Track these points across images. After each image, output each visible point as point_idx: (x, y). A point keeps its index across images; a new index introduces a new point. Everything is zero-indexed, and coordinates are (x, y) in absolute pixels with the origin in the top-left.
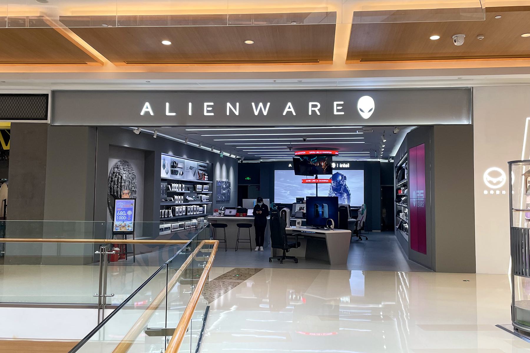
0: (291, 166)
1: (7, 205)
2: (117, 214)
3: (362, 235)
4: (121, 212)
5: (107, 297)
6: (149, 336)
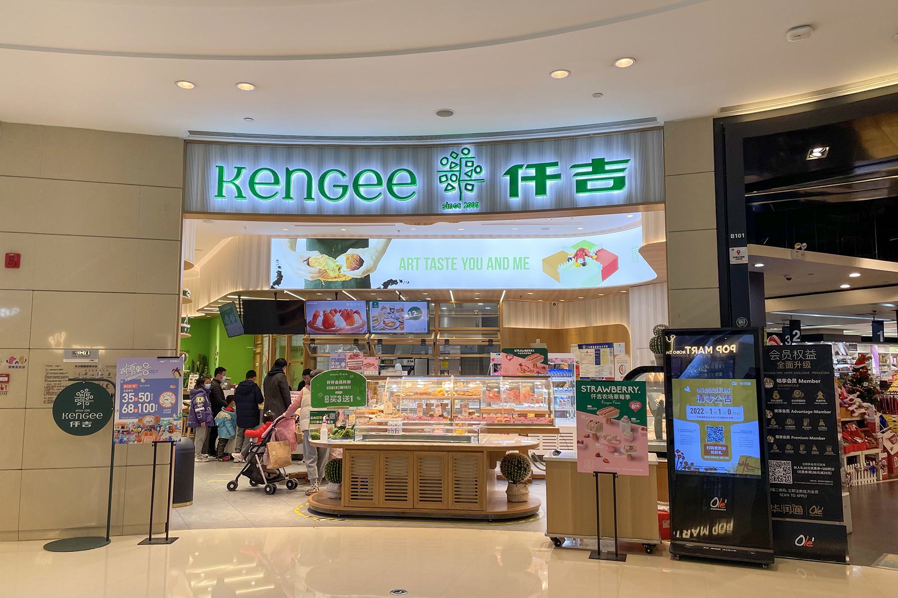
0: (685, 389)
1: (193, 370)
2: (123, 411)
3: (454, 170)
4: (131, 407)
5: (158, 443)
6: (247, 373)
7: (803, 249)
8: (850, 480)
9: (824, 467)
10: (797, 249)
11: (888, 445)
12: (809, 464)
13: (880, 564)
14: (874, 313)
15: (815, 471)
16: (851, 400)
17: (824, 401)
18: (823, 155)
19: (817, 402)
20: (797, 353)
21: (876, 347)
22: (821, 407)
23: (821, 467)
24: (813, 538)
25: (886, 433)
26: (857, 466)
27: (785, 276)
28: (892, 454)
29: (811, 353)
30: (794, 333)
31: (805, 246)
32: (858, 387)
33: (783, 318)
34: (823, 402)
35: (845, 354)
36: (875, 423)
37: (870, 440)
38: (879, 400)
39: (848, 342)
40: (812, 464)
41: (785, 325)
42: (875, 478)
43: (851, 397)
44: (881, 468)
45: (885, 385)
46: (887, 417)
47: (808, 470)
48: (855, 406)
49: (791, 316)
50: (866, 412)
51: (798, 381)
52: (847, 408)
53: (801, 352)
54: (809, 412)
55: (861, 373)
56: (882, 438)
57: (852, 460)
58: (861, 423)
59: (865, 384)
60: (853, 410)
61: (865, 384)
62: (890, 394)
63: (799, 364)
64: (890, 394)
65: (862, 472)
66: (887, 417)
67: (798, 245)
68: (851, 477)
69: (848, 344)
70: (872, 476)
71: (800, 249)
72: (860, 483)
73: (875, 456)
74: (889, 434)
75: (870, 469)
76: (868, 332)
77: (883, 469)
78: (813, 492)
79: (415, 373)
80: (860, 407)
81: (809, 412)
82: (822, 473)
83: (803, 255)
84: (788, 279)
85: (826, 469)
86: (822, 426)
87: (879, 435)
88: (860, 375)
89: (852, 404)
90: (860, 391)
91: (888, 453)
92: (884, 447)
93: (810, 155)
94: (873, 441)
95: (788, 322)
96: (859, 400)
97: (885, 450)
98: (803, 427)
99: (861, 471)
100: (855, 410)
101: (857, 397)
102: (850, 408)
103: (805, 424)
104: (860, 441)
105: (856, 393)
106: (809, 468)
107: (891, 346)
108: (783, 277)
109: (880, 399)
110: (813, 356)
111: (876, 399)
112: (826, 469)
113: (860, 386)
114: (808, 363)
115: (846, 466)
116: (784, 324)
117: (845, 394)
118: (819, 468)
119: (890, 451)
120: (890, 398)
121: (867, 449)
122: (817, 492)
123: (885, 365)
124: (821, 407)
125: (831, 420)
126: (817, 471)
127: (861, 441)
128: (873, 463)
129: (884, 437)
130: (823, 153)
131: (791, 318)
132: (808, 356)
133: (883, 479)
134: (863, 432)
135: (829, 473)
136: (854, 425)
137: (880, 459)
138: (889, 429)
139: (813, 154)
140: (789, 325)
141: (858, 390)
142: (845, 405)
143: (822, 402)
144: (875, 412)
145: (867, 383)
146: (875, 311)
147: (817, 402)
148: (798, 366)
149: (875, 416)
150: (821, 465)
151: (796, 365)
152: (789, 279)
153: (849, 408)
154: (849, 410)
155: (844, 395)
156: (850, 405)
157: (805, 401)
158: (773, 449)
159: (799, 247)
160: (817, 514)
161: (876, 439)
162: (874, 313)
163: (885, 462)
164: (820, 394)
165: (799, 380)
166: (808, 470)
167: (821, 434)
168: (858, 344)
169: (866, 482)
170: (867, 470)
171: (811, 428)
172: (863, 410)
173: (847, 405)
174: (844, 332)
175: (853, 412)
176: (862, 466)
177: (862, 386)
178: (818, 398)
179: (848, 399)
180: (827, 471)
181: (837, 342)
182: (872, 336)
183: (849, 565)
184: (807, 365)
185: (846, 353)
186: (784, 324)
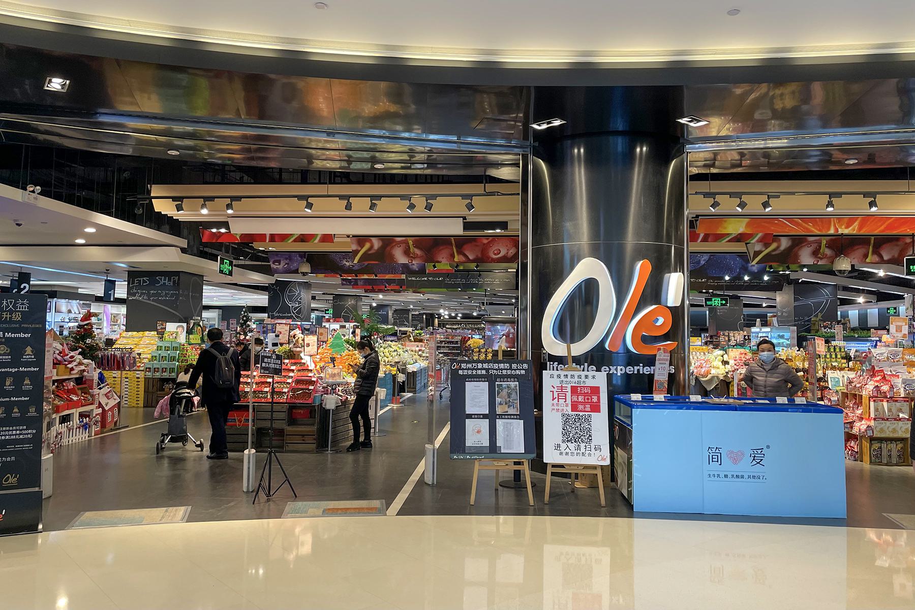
7: (36, 193)
8: (61, 440)
9: (24, 430)
10: (30, 192)
11: (103, 401)
12: (8, 428)
13: (74, 525)
14: (107, 272)
15: (13, 435)
16: (72, 357)
17: (33, 357)
18: (62, 88)
19: (25, 358)
20: (7, 303)
21: (109, 306)
22: (28, 364)
23: (20, 430)
24: (4, 510)
25: (103, 389)
26: (70, 425)
27: (15, 220)
28: (107, 409)
29: (23, 304)
30: (22, 287)
31: (39, 189)
32: (81, 344)
33: (13, 269)
34: (31, 358)
35: (77, 312)
36: (93, 380)
37: (86, 397)
38: (100, 357)
39: (82, 300)
40: (11, 428)
41: (14, 278)
42: (87, 434)
43: (72, 354)
44: (94, 424)
45: (110, 342)
46: (106, 374)
47: (5, 435)
48: (75, 363)
49: (21, 267)
50: (86, 368)
51: (4, 335)
52: (66, 365)
53: (11, 302)
54: (14, 370)
55: (85, 330)
56: (98, 394)
57: (65, 419)
58: (80, 381)
59: (88, 341)
60: (72, 367)
61: (88, 341)
62: (112, 351)
63: (8, 316)
64: (112, 351)
65: (74, 430)
66: (106, 374)
67: (32, 187)
68: (62, 436)
69: (81, 302)
70: (84, 433)
71: (33, 192)
72: (70, 442)
73: (90, 412)
74: (106, 390)
75: (82, 426)
76: (100, 292)
77: (96, 425)
78: (9, 459)
79: (60, 373)
80: (80, 364)
81: (14, 370)
82: (21, 437)
83: (36, 199)
84: (17, 224)
85: (26, 432)
86: (27, 385)
87: (96, 391)
88: (84, 333)
89: (72, 361)
90: (82, 348)
91: (103, 408)
92: (100, 403)
93: (48, 84)
94: (89, 397)
95: (17, 275)
96: (80, 357)
97: (100, 405)
98: (5, 387)
99: (73, 429)
100: (74, 367)
101: (79, 354)
102: (70, 366)
103: (8, 383)
104: (75, 398)
105: (78, 350)
106: (7, 433)
107: (122, 307)
108: (13, 222)
109: (101, 356)
110: (25, 307)
111: (97, 355)
112: (26, 432)
113: (83, 343)
114: (18, 314)
115: (57, 426)
116: (13, 276)
117: (67, 351)
118: (18, 432)
119: (105, 406)
120: (111, 354)
121: (82, 406)
122: (13, 458)
123: (116, 325)
124: (28, 364)
125: (38, 378)
126: (16, 435)
127: (76, 398)
128: (86, 420)
129: (100, 393)
130: (63, 86)
131: (21, 270)
132: (20, 307)
133: (95, 435)
134: (81, 389)
135: (29, 436)
136: (71, 383)
137: (94, 416)
138: (106, 385)
139: (51, 84)
140: (17, 278)
141: (80, 347)
142: (65, 363)
143: (29, 358)
144: (95, 368)
145: (90, 340)
146: (107, 270)
147: (25, 358)
148: (6, 317)
149: (94, 373)
150: (21, 428)
151: (5, 316)
152: (19, 225)
153: (69, 366)
154: (68, 368)
155: (65, 352)
156: (70, 362)
157: (10, 357)
158: (30, 413)
159: (32, 189)
160: (12, 483)
161: (93, 396)
162: (107, 272)
163: (99, 418)
164: (29, 350)
165: (6, 333)
166: (5, 435)
167: (25, 393)
168: (92, 304)
169: (77, 440)
170: (79, 428)
171: (14, 387)
172: (83, 367)
173: (66, 363)
174: (79, 290)
175: (72, 369)
176: (75, 424)
177: (85, 343)
178: (26, 354)
179: (68, 357)
180: (27, 434)
181: (71, 299)
182: (103, 295)
183: (41, 532)
184: (17, 317)
185: (79, 311)
186: (13, 276)
